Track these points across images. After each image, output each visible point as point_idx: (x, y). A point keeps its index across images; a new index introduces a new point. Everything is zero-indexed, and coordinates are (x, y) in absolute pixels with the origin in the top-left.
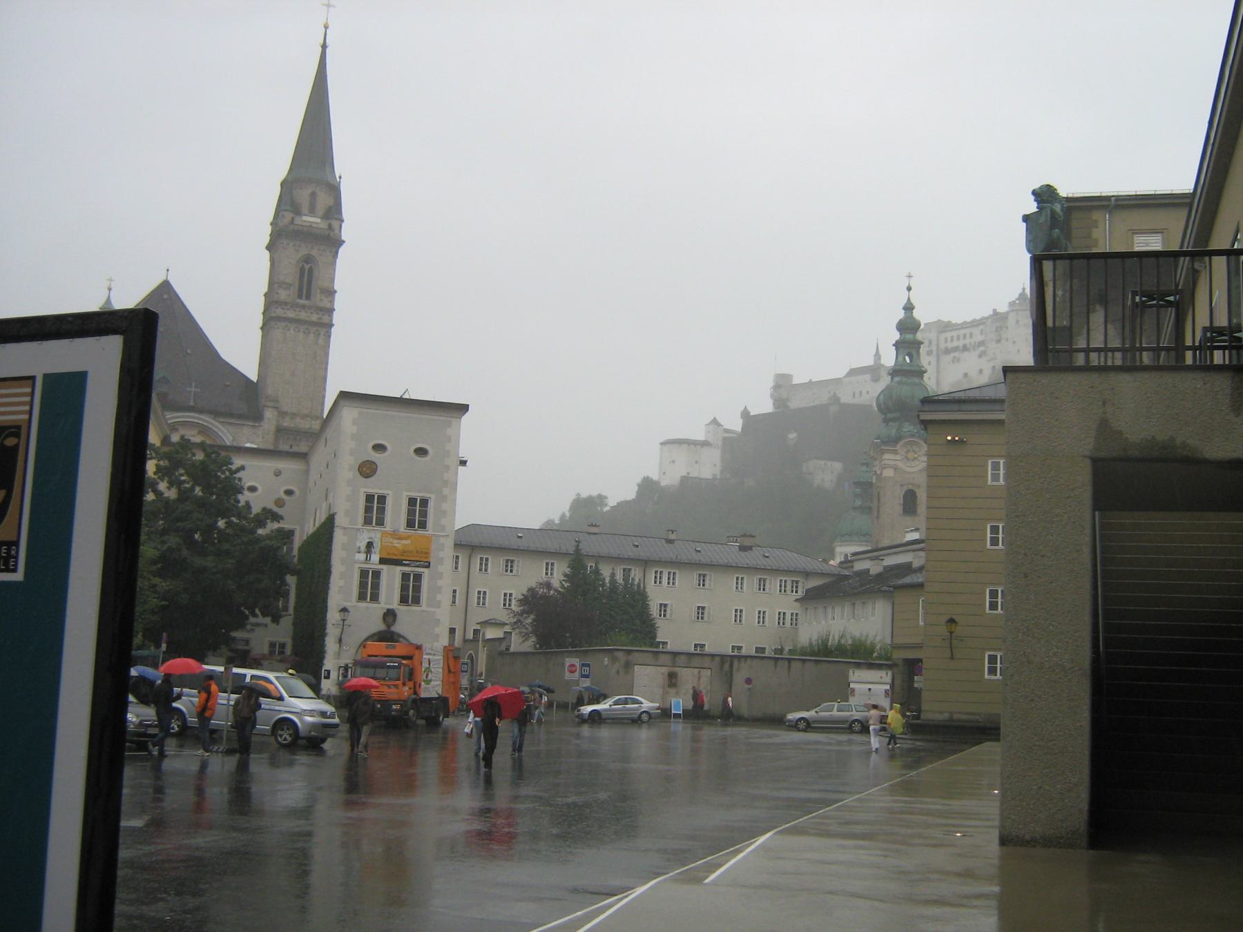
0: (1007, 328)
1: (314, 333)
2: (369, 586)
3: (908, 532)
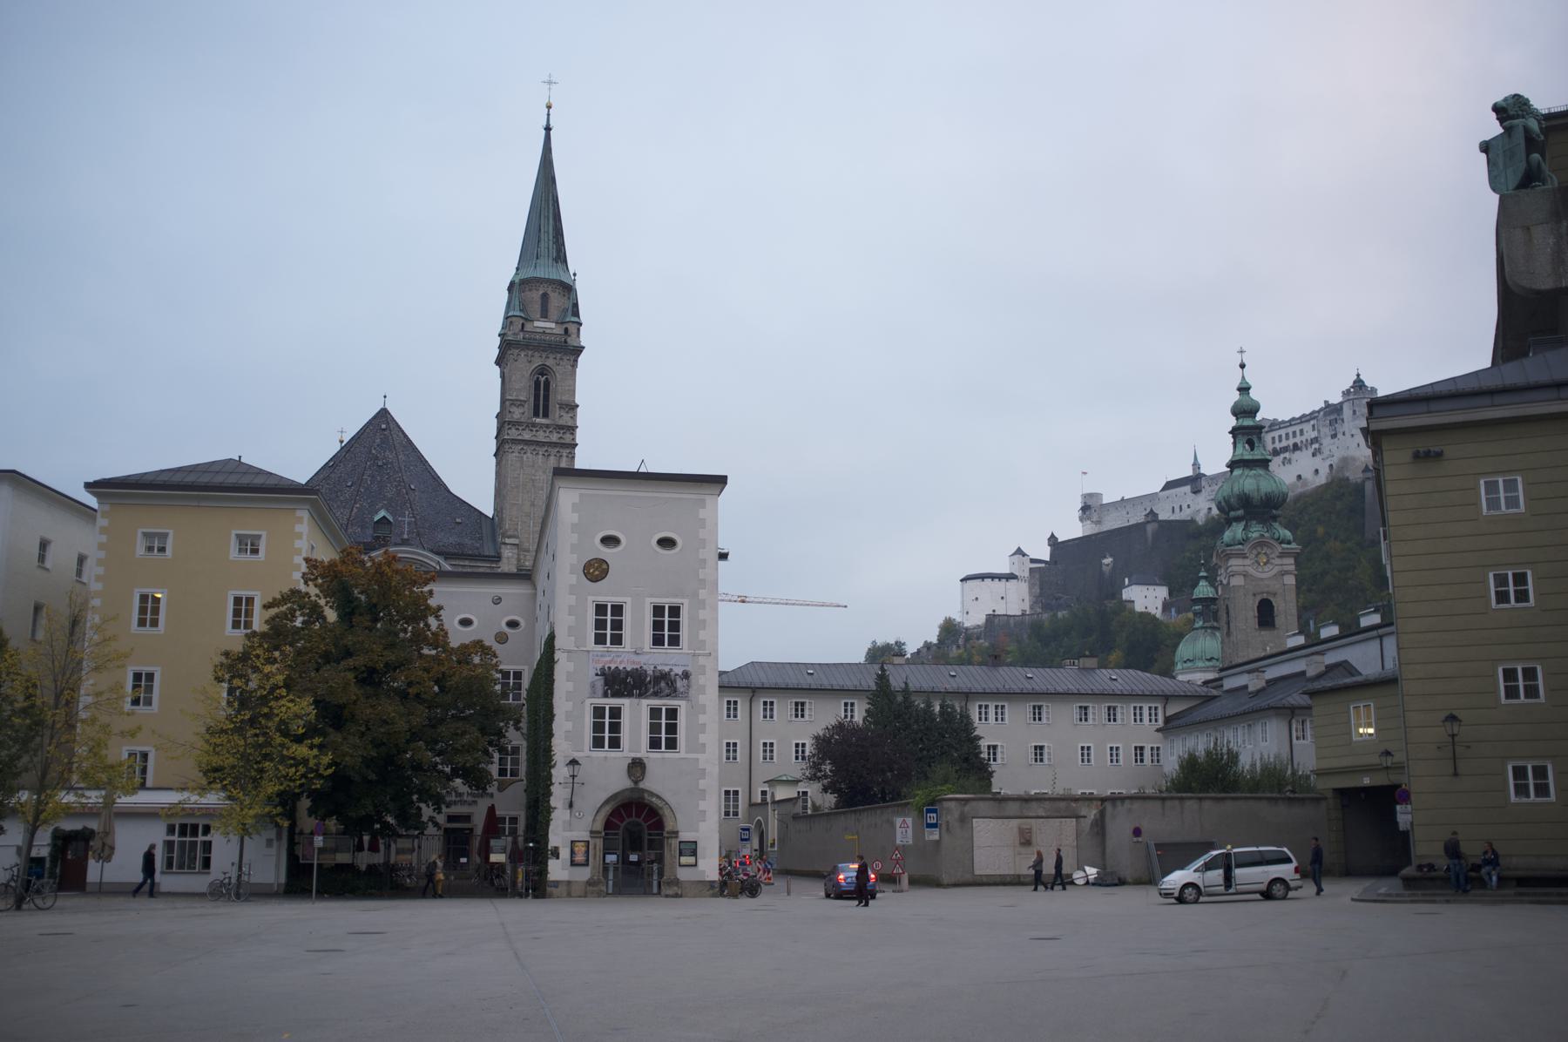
0: (1343, 420)
1: (555, 455)
2: (607, 731)
3: (1289, 636)
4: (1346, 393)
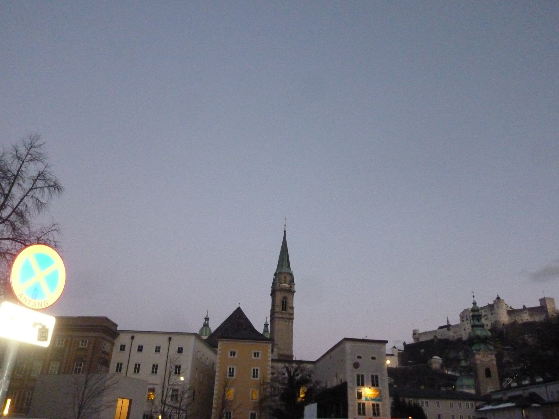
4: (495, 301)
